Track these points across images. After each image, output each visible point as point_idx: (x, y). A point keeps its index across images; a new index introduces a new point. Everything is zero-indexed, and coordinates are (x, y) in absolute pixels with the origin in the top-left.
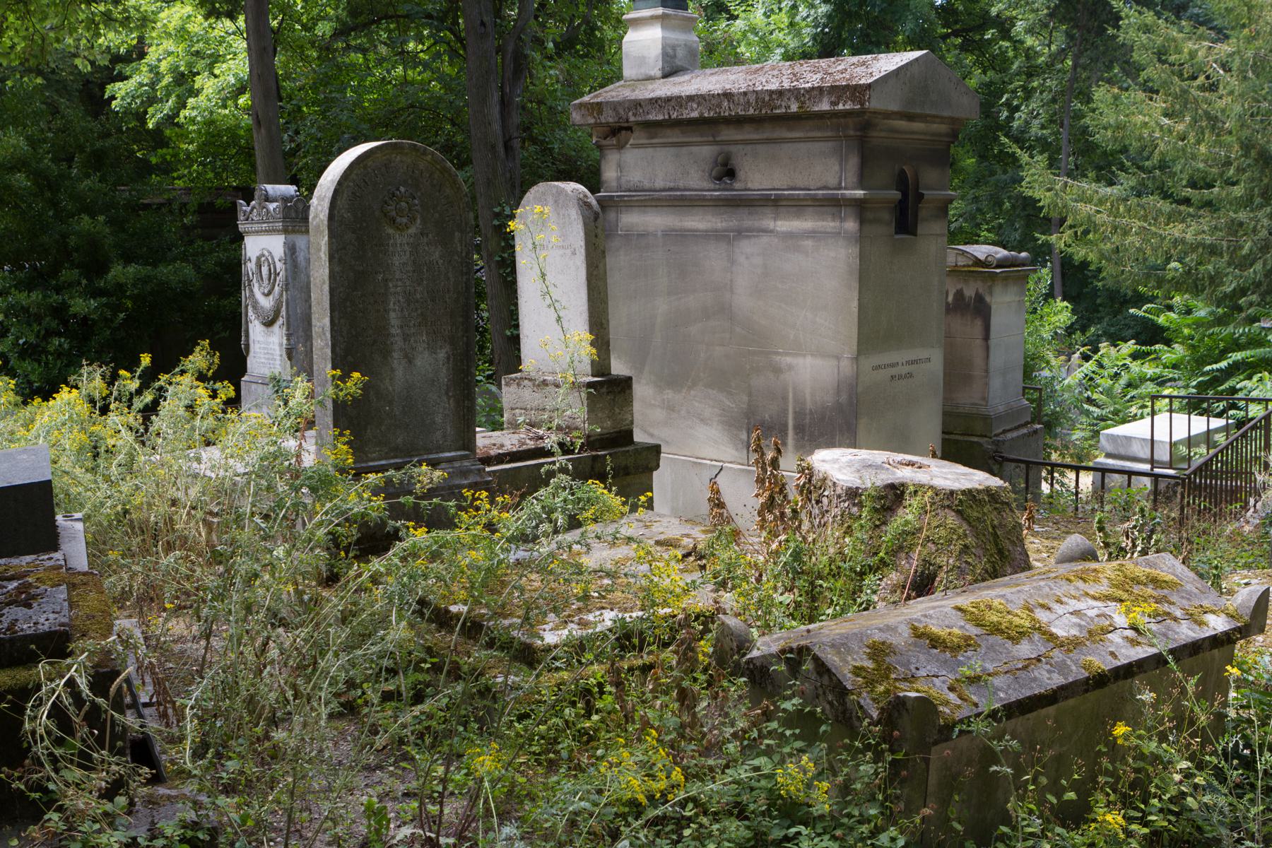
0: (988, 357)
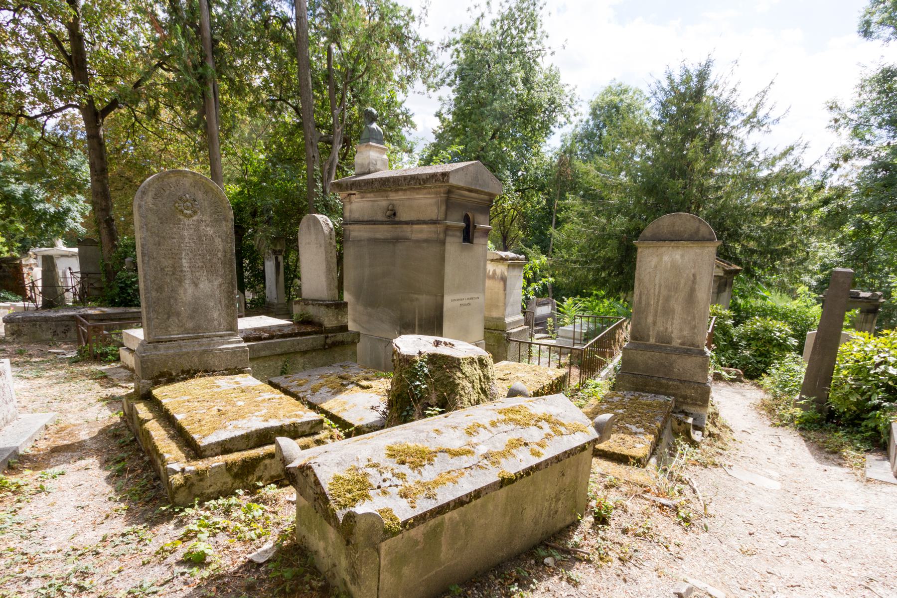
0: (505, 298)
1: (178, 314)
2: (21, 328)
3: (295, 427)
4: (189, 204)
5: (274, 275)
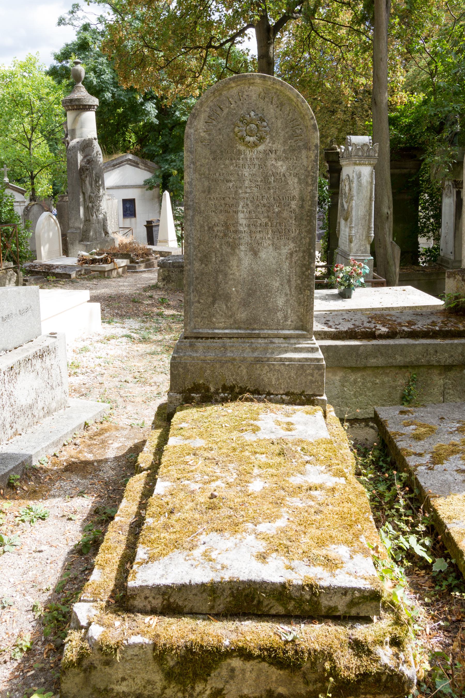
1: (227, 298)
2: (170, 273)
3: (314, 594)
4: (253, 126)
5: (453, 219)
